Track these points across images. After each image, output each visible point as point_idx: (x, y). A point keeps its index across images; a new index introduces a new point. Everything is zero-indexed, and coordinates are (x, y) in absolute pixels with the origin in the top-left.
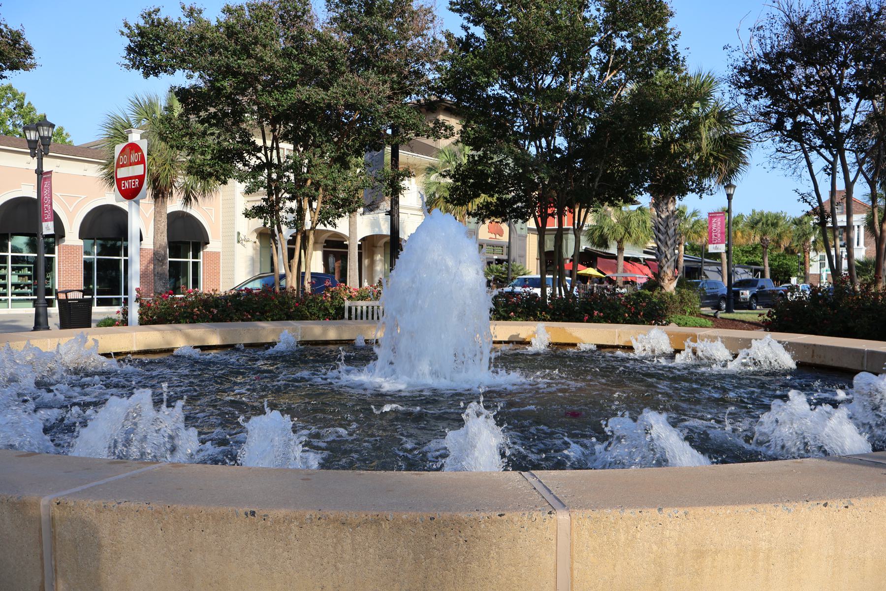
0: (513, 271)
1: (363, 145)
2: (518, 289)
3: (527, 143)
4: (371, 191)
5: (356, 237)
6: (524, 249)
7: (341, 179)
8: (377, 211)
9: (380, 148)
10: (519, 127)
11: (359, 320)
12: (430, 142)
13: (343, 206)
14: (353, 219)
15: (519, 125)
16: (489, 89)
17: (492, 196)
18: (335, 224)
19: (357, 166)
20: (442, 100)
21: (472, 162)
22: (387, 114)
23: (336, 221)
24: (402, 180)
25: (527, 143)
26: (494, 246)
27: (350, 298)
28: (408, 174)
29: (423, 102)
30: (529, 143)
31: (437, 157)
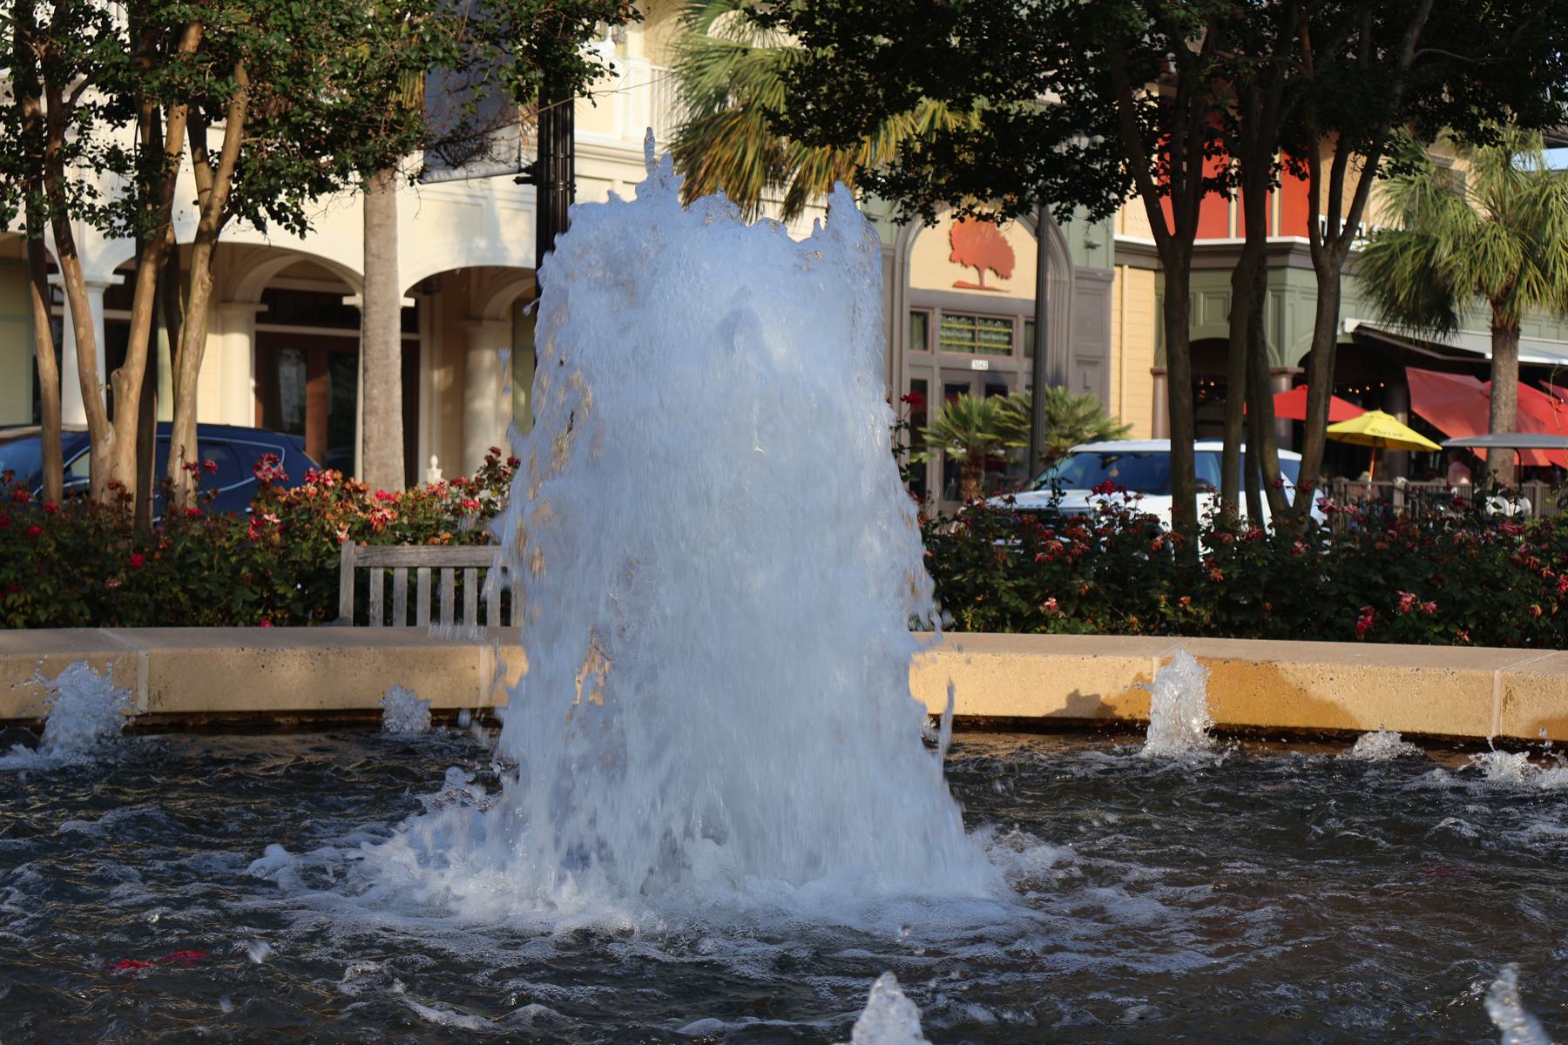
0: (1053, 421)
2: (1075, 500)
4: (456, 79)
5: (392, 279)
8: (478, 168)
11: (376, 629)
23: (308, 207)
24: (588, 33)
26: (977, 318)
27: (365, 532)
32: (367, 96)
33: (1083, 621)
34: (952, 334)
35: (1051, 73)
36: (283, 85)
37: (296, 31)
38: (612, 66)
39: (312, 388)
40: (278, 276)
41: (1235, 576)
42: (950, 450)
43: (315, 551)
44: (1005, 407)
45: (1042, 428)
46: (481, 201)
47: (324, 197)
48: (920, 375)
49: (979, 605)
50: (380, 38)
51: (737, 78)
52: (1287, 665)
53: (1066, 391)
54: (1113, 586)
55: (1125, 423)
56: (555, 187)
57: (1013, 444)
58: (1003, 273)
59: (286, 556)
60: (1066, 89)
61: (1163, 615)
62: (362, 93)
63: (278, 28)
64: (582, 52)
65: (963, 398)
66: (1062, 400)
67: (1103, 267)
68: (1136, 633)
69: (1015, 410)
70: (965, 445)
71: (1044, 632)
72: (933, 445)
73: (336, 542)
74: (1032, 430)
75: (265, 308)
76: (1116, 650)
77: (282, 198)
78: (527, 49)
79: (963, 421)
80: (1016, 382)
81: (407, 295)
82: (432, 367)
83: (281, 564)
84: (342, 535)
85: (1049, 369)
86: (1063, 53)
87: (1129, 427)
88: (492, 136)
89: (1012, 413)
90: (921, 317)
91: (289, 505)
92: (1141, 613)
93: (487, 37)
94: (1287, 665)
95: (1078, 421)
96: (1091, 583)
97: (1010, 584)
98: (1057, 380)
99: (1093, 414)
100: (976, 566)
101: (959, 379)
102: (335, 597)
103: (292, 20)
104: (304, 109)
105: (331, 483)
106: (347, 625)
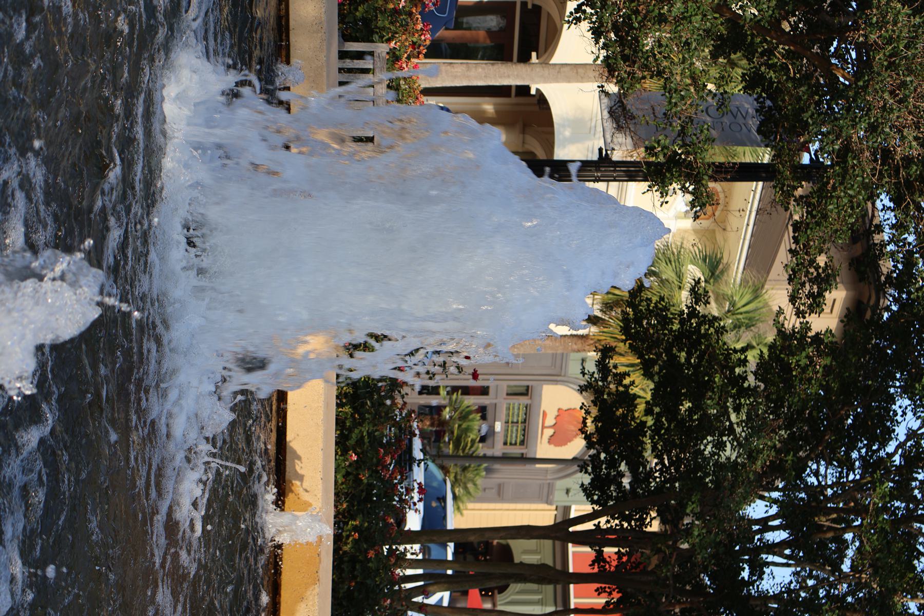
0: (465, 469)
1: (774, 93)
2: (418, 474)
3: (775, 495)
4: (660, 111)
5: (546, 80)
6: (520, 496)
7: (685, 36)
8: (609, 125)
9: (768, 131)
10: (816, 474)
11: (336, 63)
12: (783, 257)
13: (621, 41)
14: (592, 74)
15: (823, 474)
16: (907, 402)
17: (648, 412)
18: (578, 20)
19: (722, 80)
20: (880, 291)
21: (727, 361)
22: (846, 149)
23: (585, 25)
24: (684, 190)
25: (775, 495)
26: (525, 425)
27: (394, 58)
28: (701, 202)
29: (877, 238)
30: (775, 501)
31: (744, 282)
32: (647, 59)
33: (344, 477)
34: (516, 410)
35: (666, 462)
36: (653, 10)
37: (684, 18)
38: (667, 203)
39: (482, 34)
40: (549, 14)
41: (370, 565)
42: (448, 409)
43: (384, 28)
44: (473, 441)
45: (460, 462)
46: (592, 132)
47: (589, 35)
48: (491, 391)
49: (352, 415)
50: (682, 66)
51: (663, 282)
52: (317, 590)
53: (482, 477)
54: (364, 494)
55: (465, 512)
56: (597, 171)
57: (451, 446)
58: (552, 440)
59: (381, 12)
60: (656, 471)
61: (347, 523)
62: (648, 57)
63: (686, 8)
64: (674, 185)
65: (478, 416)
66: (477, 474)
67: (555, 499)
68: (336, 507)
69: (471, 447)
70: (451, 417)
71: (336, 454)
72: (450, 399)
73: (389, 41)
74: (459, 457)
75: (530, 6)
76: (325, 490)
77: (589, 10)
78: (675, 153)
79: (464, 417)
80: (488, 448)
81: (538, 90)
82: (495, 104)
83: (376, 9)
84: (392, 44)
85: (497, 466)
86: (677, 470)
87: (462, 514)
88: (628, 133)
89: (469, 445)
90: (526, 392)
91: (410, 14)
92: (348, 510)
93: (683, 128)
94: (317, 590)
95: (465, 484)
96: (365, 481)
97: (365, 434)
98: (488, 470)
99: (468, 493)
100: (376, 414)
101: (490, 415)
102: (356, 40)
103: (691, 16)
104: (639, 23)
105: (423, 38)
106: (339, 46)
